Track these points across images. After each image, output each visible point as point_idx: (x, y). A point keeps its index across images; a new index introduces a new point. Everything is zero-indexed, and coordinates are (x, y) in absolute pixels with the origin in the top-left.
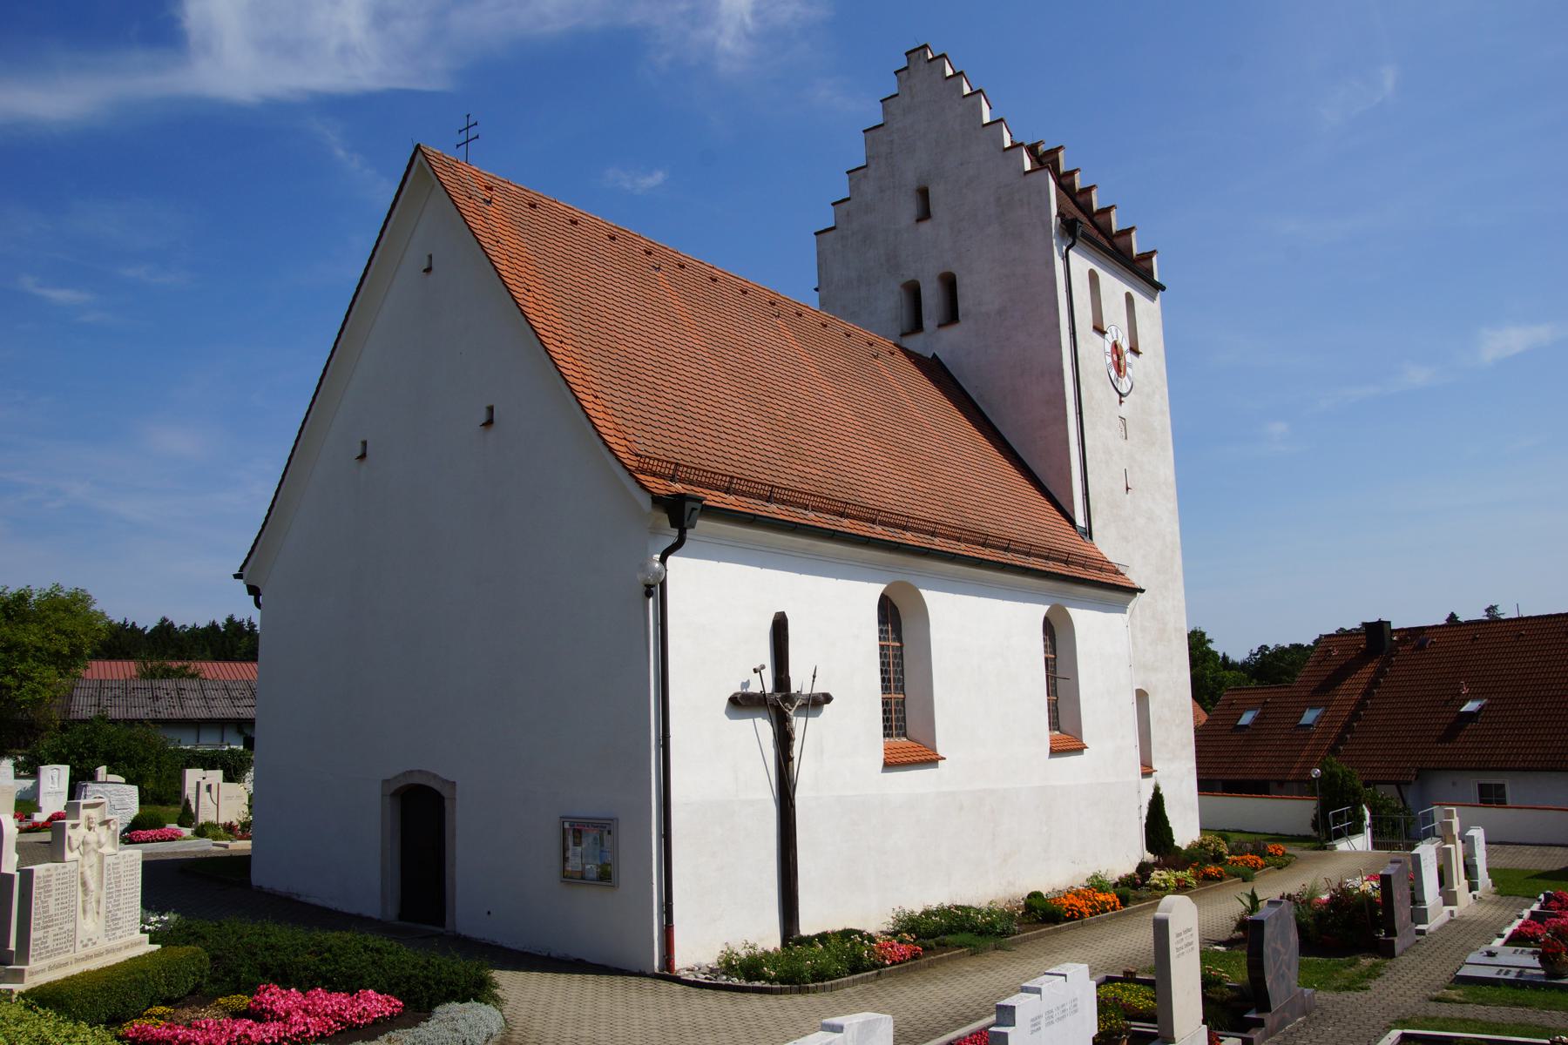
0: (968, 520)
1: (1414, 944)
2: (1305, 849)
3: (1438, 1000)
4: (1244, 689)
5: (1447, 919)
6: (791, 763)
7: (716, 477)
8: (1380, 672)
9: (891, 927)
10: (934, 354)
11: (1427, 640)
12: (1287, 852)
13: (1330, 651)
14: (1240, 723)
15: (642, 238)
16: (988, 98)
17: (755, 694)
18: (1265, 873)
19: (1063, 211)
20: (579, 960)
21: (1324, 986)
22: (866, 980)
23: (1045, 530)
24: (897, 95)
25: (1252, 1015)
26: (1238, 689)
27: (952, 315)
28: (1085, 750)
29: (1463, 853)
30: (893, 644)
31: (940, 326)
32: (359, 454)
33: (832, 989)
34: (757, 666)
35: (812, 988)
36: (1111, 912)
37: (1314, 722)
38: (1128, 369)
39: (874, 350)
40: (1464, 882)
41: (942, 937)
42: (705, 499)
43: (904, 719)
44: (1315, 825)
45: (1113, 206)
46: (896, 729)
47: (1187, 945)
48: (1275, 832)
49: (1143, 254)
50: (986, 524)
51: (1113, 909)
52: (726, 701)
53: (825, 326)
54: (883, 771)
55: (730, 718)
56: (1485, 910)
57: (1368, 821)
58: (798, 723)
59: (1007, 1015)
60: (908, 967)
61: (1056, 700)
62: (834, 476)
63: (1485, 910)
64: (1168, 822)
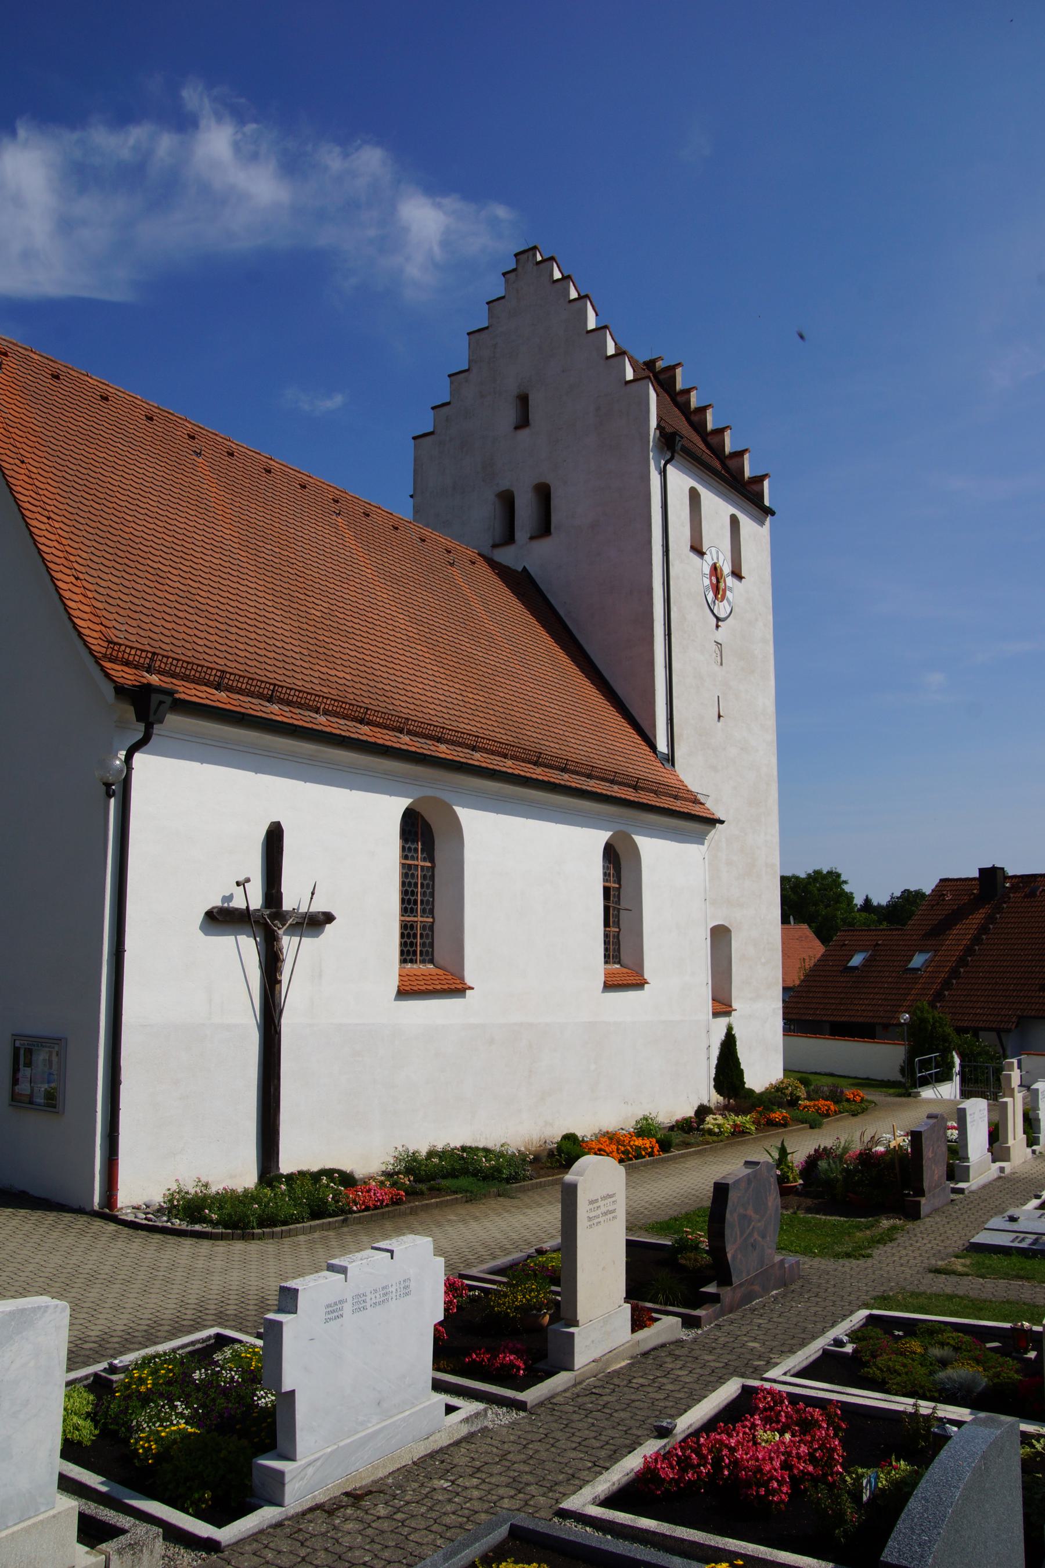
0: (525, 738)
1: (947, 1205)
2: (890, 1095)
3: (938, 1271)
4: (857, 930)
5: (996, 1176)
6: (278, 986)
7: (301, 695)
8: (991, 919)
9: (391, 1167)
10: (524, 567)
11: (1039, 887)
12: (866, 1097)
13: (944, 895)
14: (850, 964)
15: (190, 423)
16: (594, 304)
17: (237, 909)
18: (838, 1120)
19: (663, 424)
20: (23, 1192)
21: (826, 1251)
22: (329, 1227)
23: (618, 753)
24: (503, 298)
25: (711, 1289)
26: (852, 930)
27: (544, 528)
28: (646, 985)
29: (1024, 1104)
30: (422, 864)
31: (532, 538)
32: (163, 705)
33: (282, 1235)
34: (241, 879)
35: (259, 1234)
36: (648, 1158)
37: (922, 966)
38: (728, 593)
39: (451, 557)
40: (1021, 1137)
41: (440, 1181)
42: (177, 692)
43: (432, 945)
44: (902, 1071)
45: (728, 427)
46: (421, 955)
47: (605, 1214)
48: (865, 1077)
49: (755, 477)
50: (547, 743)
51: (651, 1154)
52: (201, 916)
53: (397, 528)
54: (395, 1000)
55: (206, 934)
56: (1040, 1167)
57: (957, 1068)
58: (288, 943)
59: (288, 1300)
60: (383, 1214)
61: (619, 932)
62: (365, 681)
63: (1040, 1167)
64: (739, 1064)
